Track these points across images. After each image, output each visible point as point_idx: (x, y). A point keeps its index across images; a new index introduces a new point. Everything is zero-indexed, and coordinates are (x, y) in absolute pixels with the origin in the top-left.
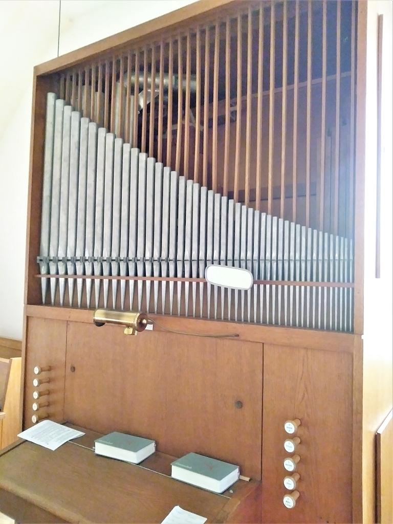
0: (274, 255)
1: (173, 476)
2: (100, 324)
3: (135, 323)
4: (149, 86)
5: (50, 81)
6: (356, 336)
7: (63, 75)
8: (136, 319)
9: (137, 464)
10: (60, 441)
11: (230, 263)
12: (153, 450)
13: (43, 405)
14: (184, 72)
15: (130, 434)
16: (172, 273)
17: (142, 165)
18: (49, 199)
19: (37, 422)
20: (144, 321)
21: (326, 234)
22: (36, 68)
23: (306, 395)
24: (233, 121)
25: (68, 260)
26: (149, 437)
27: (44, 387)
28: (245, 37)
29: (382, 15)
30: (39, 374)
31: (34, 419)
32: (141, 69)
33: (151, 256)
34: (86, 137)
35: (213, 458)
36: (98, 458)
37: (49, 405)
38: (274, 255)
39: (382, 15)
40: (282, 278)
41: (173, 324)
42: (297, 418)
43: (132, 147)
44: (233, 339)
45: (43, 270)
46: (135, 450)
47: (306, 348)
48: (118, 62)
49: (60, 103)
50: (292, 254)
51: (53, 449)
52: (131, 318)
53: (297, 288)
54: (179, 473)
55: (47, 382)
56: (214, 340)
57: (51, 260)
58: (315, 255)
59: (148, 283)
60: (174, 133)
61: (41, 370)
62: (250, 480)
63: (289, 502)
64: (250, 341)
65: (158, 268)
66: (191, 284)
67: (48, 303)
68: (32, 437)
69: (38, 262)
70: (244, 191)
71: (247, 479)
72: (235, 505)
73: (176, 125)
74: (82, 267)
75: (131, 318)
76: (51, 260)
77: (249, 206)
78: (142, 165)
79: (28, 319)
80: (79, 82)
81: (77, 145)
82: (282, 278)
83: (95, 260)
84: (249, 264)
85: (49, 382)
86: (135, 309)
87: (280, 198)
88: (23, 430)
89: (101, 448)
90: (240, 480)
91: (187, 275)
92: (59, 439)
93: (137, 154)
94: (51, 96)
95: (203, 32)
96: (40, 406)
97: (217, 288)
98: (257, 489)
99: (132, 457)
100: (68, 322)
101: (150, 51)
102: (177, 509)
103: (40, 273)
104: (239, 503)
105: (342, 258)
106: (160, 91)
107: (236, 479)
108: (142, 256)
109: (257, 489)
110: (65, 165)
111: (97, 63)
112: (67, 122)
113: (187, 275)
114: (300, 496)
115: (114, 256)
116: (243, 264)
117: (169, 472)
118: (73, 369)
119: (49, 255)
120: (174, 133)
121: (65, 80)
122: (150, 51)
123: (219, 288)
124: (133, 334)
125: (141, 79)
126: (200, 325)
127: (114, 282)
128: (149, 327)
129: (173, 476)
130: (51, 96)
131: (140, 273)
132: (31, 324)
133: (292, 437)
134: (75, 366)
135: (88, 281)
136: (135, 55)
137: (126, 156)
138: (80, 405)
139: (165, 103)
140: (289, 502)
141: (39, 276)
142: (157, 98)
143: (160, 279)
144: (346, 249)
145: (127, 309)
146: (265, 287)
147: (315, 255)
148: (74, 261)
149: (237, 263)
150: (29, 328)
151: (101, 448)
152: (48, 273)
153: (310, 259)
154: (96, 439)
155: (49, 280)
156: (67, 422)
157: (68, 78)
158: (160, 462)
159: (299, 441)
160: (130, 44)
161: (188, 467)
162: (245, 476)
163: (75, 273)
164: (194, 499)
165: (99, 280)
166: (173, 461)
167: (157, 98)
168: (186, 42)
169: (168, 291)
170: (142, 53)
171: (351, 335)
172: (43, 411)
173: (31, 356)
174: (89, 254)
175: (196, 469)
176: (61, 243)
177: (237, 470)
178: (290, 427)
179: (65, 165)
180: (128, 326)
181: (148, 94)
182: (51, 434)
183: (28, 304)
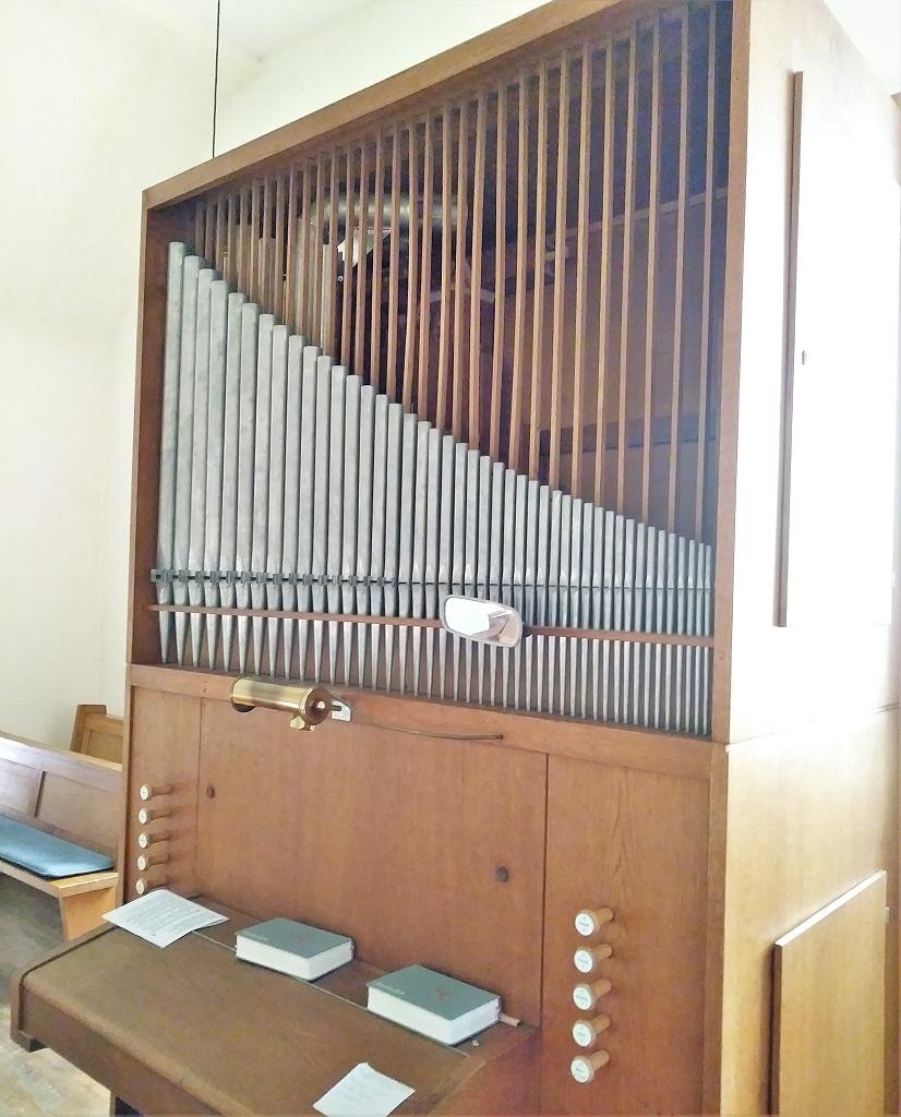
0: (575, 576)
1: (371, 1007)
2: (243, 708)
3: (303, 707)
4: (369, 223)
5: (176, 219)
6: (716, 746)
7: (202, 203)
8: (305, 699)
9: (310, 982)
10: (177, 930)
11: (469, 590)
12: (348, 957)
13: (158, 860)
14: (437, 190)
15: (305, 921)
16: (389, 609)
17: (337, 390)
18: (172, 454)
19: (145, 893)
20: (321, 705)
21: (682, 540)
22: (146, 193)
23: (623, 863)
24: (549, 281)
25: (191, 578)
26: (340, 931)
27: (161, 825)
28: (455, 146)
29: (801, 73)
30: (148, 799)
31: (140, 886)
32: (342, 189)
33: (352, 574)
34: (237, 331)
35: (451, 976)
36: (240, 966)
37: (169, 860)
38: (575, 576)
39: (801, 73)
40: (588, 625)
41: (395, 712)
42: (604, 907)
43: (320, 353)
44: (492, 744)
45: (163, 597)
46: (306, 952)
47: (626, 769)
48: (300, 177)
49: (192, 262)
50: (608, 575)
51: (163, 946)
52: (295, 698)
53: (617, 644)
54: (382, 1002)
55: (167, 816)
56: (459, 744)
57: (175, 577)
58: (650, 579)
59: (347, 627)
60: (435, 308)
61: (154, 793)
62: (519, 1024)
63: (581, 1070)
64: (522, 749)
65: (365, 597)
66: (423, 631)
67: (171, 662)
68: (128, 921)
69: (153, 580)
70: (549, 432)
71: (514, 1022)
72: (474, 1066)
73: (437, 293)
74: (231, 590)
75: (295, 698)
76: (175, 577)
77: (519, 473)
78: (337, 390)
79: (133, 690)
80: (230, 216)
81: (222, 349)
82: (588, 625)
83: (253, 579)
84: (519, 594)
85: (170, 815)
86: (309, 680)
87: (643, 445)
88: (125, 902)
89: (248, 948)
90: (499, 1023)
91: (417, 613)
92: (175, 927)
93: (328, 368)
94: (176, 249)
95: (456, 114)
96: (151, 862)
97: (471, 644)
98: (530, 1041)
99: (301, 967)
100: (202, 701)
101: (357, 153)
102: (363, 1070)
103: (156, 603)
104: (483, 1064)
105: (700, 586)
106: (392, 230)
107: (493, 1019)
108: (337, 574)
109: (530, 1041)
110: (200, 386)
111: (262, 179)
112: (203, 301)
113: (417, 613)
114: (609, 1062)
115: (317, 572)
116: (494, 592)
117: (363, 1000)
118: (212, 793)
119: (172, 567)
120: (435, 308)
121: (205, 213)
122: (357, 153)
123: (462, 641)
124: (306, 728)
125: (344, 209)
126: (436, 714)
127: (288, 623)
128: (343, 714)
129: (371, 1007)
130: (176, 249)
131: (333, 607)
132: (140, 702)
133: (591, 943)
134: (215, 786)
135: (242, 620)
136: (496, 97)
137: (309, 371)
138: (223, 863)
139: (403, 255)
140: (581, 1070)
141: (155, 608)
142: (386, 242)
143: (396, 621)
144: (708, 568)
145: (294, 679)
146: (557, 641)
147: (650, 579)
148: (217, 578)
149: (494, 592)
150: (136, 713)
151: (248, 948)
152: (172, 602)
153: (641, 586)
154: (240, 929)
155: (172, 617)
156: (199, 897)
157: (210, 211)
158: (349, 982)
159: (608, 951)
160: (383, 114)
161: (397, 991)
162: (510, 1016)
163: (219, 604)
164: (397, 1052)
165: (260, 619)
166: (373, 977)
167: (386, 242)
168: (651, 48)
169: (384, 644)
170: (342, 160)
171: (706, 744)
172: (157, 873)
173: (139, 761)
174: (243, 567)
175: (413, 997)
176: (194, 543)
177: (495, 1003)
178: (585, 924)
179: (200, 386)
180: (296, 713)
181: (366, 240)
182: (162, 917)
183: (132, 663)
